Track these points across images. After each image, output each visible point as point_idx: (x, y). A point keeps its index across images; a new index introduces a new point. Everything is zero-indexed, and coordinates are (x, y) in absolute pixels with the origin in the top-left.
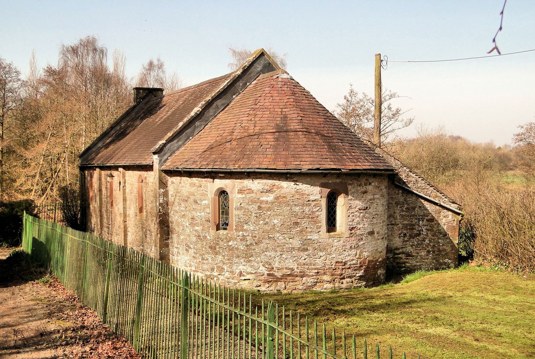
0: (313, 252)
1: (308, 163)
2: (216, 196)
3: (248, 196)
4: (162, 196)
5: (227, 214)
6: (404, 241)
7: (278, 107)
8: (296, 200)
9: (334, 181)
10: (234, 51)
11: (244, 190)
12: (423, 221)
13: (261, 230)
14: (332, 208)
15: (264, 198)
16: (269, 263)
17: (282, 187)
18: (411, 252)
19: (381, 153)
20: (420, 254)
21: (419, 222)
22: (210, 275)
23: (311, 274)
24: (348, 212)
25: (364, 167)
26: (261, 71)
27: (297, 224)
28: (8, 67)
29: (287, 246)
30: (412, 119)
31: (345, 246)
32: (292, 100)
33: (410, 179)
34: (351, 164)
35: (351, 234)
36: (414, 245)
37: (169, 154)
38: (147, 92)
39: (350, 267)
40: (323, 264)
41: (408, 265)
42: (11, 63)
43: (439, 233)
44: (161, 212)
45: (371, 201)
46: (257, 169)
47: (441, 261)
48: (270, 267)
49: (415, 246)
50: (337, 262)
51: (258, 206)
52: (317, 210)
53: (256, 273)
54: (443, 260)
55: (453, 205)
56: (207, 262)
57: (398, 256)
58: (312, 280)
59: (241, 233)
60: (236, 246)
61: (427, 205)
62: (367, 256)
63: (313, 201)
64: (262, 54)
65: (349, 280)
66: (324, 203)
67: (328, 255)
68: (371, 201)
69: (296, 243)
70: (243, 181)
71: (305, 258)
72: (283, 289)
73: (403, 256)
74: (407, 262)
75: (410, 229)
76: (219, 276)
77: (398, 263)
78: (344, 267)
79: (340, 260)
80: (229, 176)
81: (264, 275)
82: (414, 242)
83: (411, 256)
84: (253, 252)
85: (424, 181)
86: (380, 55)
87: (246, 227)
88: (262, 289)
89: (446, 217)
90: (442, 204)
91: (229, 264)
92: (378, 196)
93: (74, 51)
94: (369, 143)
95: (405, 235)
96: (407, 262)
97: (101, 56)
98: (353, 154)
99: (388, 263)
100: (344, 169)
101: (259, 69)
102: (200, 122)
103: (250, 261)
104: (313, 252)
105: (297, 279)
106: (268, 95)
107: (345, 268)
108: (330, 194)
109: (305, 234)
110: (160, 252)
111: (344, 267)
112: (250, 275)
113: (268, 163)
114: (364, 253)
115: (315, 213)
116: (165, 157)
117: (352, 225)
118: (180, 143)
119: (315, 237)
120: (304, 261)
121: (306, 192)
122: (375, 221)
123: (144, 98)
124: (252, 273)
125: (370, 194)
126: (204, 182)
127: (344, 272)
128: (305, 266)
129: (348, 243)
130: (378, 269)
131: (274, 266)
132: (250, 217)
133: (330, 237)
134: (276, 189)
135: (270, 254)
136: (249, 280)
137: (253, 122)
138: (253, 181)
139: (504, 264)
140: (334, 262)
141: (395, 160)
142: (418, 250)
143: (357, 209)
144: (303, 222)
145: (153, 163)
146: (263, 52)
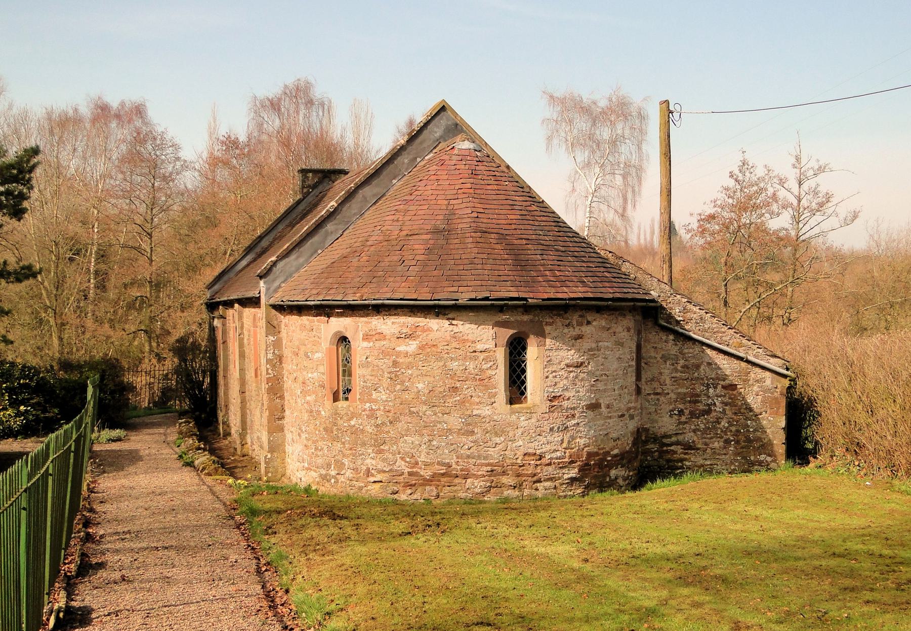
0: (484, 437)
1: (471, 289)
2: (333, 345)
3: (378, 344)
4: (272, 347)
5: (350, 375)
6: (680, 423)
7: (444, 197)
8: (454, 350)
9: (519, 318)
10: (551, 97)
11: (372, 335)
12: (715, 388)
13: (398, 401)
14: (519, 363)
15: (402, 348)
16: (411, 455)
17: (430, 330)
18: (694, 442)
19: (633, 272)
20: (711, 445)
21: (708, 389)
22: (326, 475)
23: (480, 473)
24: (546, 370)
25: (572, 295)
26: (441, 137)
27: (455, 389)
28: (160, 137)
29: (439, 426)
30: (857, 211)
31: (540, 427)
32: (469, 186)
33: (689, 315)
34: (548, 289)
35: (553, 406)
36: (699, 430)
37: (282, 279)
38: (320, 175)
39: (551, 463)
40: (501, 458)
41: (687, 463)
42: (163, 130)
43: (746, 408)
44: (270, 374)
45: (592, 353)
46: (388, 300)
47: (752, 458)
48: (413, 461)
49: (701, 431)
50: (525, 455)
51: (393, 361)
52: (489, 366)
53: (391, 470)
54: (756, 457)
55: (772, 360)
56: (321, 453)
57: (669, 448)
58: (482, 483)
59: (368, 405)
60: (361, 427)
61: (722, 361)
62: (584, 445)
63: (481, 352)
64: (443, 109)
65: (548, 484)
66: (501, 355)
67: (510, 443)
68: (592, 353)
69: (454, 421)
70: (370, 320)
71: (470, 446)
72: (434, 498)
73: (679, 449)
74: (686, 460)
75: (690, 402)
76: (337, 476)
77: (668, 461)
78: (538, 463)
79: (531, 451)
80: (350, 312)
81: (403, 474)
82: (698, 425)
83: (694, 449)
84: (385, 436)
85: (716, 319)
86: (667, 102)
87: (375, 395)
88: (403, 497)
89: (761, 381)
90: (751, 358)
91: (351, 457)
92: (609, 344)
93: (274, 105)
94: (611, 254)
95: (681, 412)
96: (686, 460)
97: (321, 113)
98: (558, 273)
99: (650, 461)
100: (533, 298)
101: (437, 135)
102: (336, 224)
103: (381, 452)
104: (484, 437)
105: (457, 481)
106: (433, 177)
107: (540, 465)
108: (515, 339)
109: (469, 406)
110: (269, 439)
111: (538, 463)
112: (383, 474)
113: (406, 290)
114: (578, 440)
115: (485, 372)
116: (276, 284)
117: (552, 392)
118: (301, 260)
119: (486, 411)
120: (468, 453)
121: (470, 337)
122: (600, 386)
123: (314, 187)
124: (385, 472)
125: (590, 341)
126: (316, 323)
127: (539, 471)
128: (470, 460)
129: (546, 422)
130: (610, 466)
131: (419, 459)
132: (381, 378)
133: (513, 412)
134: (420, 333)
135: (413, 439)
136: (381, 482)
137: (400, 223)
138: (384, 320)
139: (857, 463)
140: (520, 454)
141: (660, 283)
142: (708, 438)
143: (562, 365)
144: (465, 387)
145: (260, 293)
146: (444, 106)
